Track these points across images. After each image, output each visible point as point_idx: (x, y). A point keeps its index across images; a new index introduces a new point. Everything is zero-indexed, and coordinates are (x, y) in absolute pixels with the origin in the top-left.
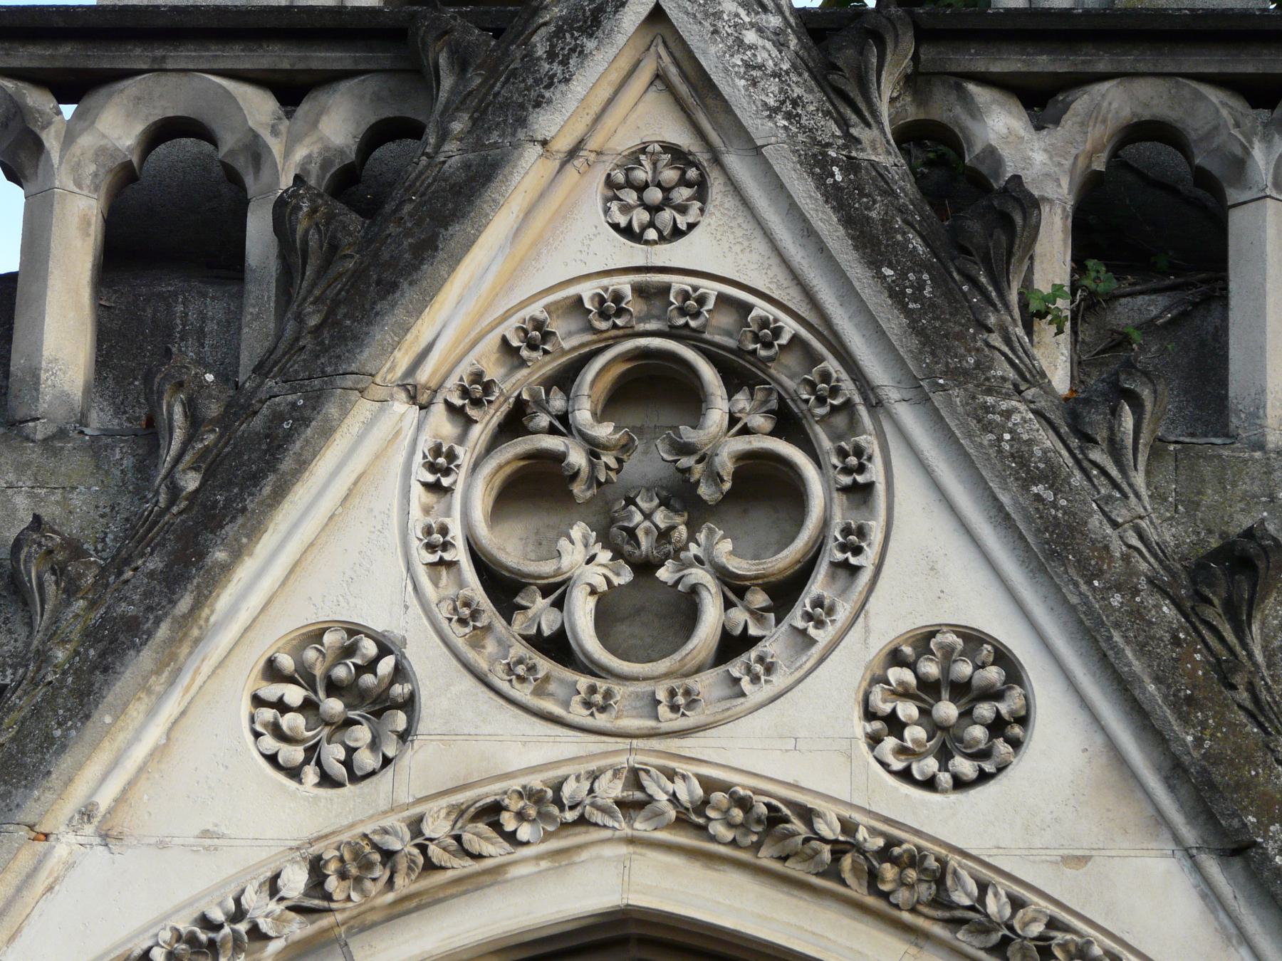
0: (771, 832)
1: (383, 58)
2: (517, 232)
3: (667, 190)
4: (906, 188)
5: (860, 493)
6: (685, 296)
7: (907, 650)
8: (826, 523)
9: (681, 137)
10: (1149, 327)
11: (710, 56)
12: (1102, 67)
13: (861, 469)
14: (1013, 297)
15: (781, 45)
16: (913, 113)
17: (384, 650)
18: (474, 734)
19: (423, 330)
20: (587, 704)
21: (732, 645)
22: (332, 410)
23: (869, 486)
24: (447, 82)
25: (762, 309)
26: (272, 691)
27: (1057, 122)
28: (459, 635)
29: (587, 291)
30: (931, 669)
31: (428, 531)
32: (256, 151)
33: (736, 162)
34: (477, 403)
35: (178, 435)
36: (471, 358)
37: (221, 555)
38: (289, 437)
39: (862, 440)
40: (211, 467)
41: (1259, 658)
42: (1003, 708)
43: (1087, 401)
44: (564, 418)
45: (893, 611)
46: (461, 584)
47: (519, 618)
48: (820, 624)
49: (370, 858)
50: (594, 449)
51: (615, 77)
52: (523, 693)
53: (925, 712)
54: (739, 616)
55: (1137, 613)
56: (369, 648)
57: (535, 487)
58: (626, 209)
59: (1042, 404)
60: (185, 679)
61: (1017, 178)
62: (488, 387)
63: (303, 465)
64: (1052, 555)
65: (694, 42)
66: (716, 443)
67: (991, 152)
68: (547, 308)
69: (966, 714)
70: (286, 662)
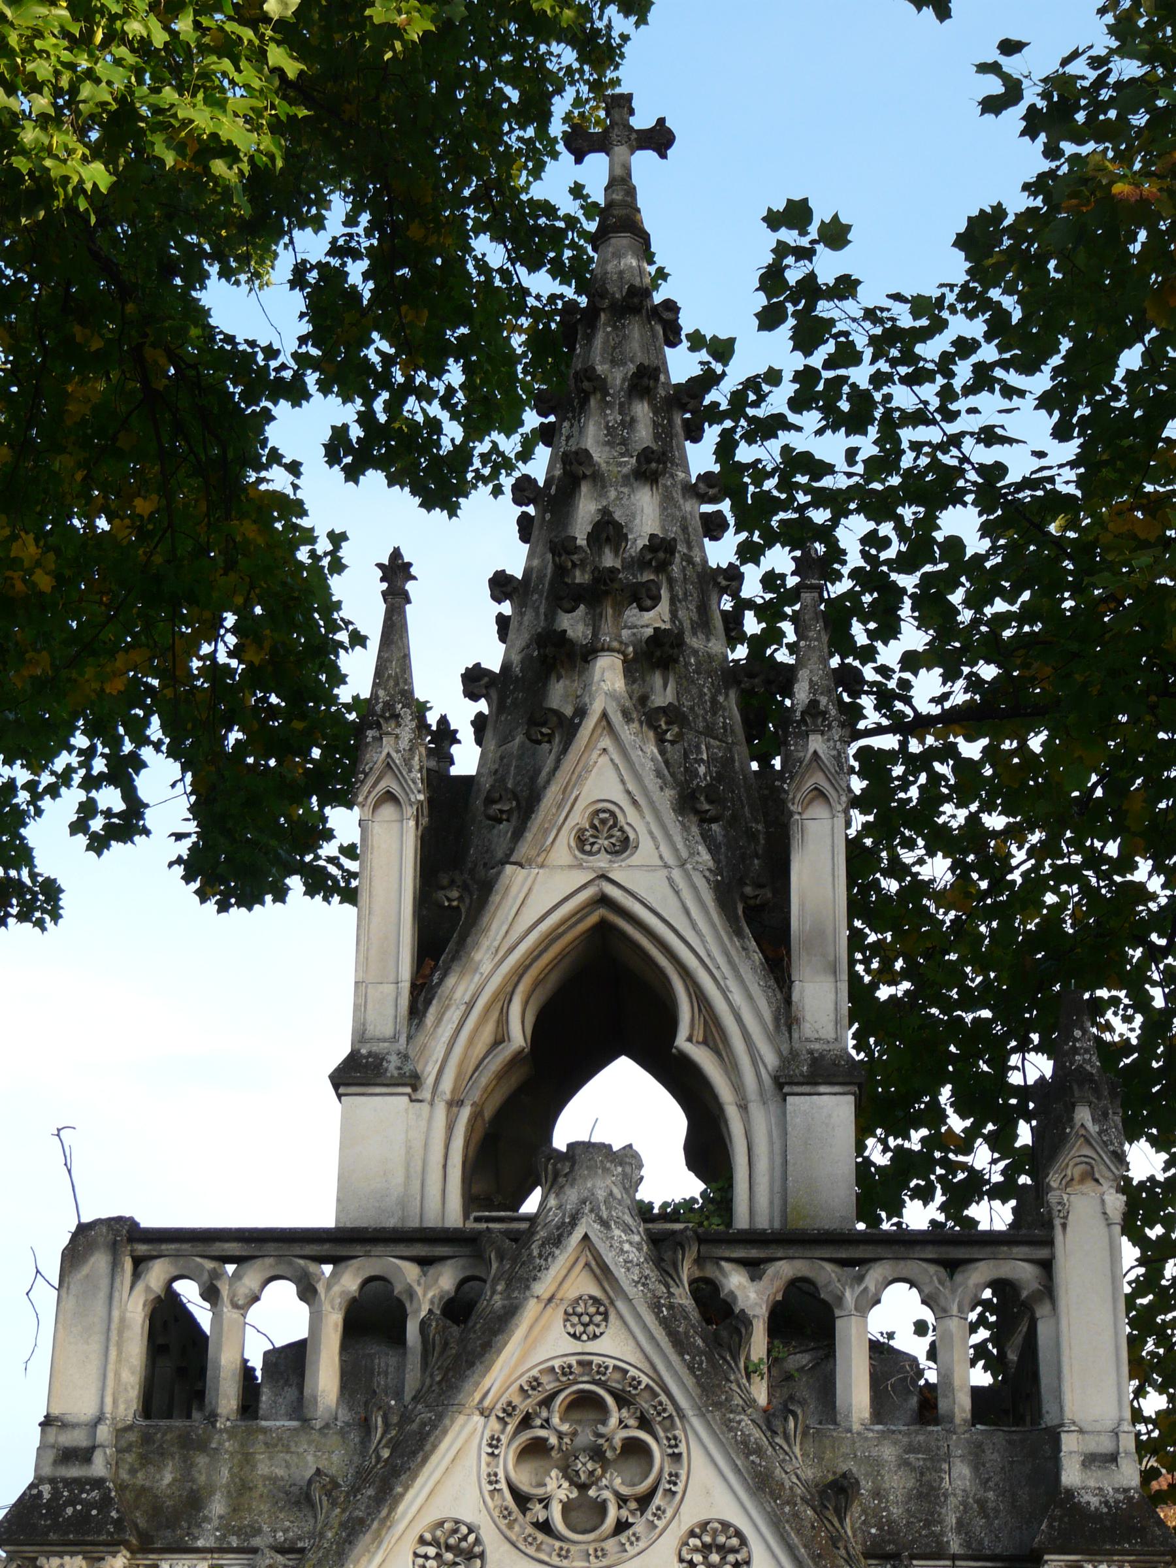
1: (466, 1250)
2: (526, 1337)
3: (591, 1317)
4: (695, 1315)
5: (676, 1457)
6: (599, 1366)
7: (697, 1530)
8: (661, 1470)
9: (597, 1292)
10: (801, 1369)
11: (609, 1258)
12: (779, 1255)
13: (676, 1446)
14: (742, 1365)
15: (639, 1250)
16: (697, 1274)
17: (471, 1531)
19: (487, 1382)
20: (559, 1555)
21: (622, 1526)
22: (447, 1421)
23: (680, 1454)
24: (495, 1265)
25: (633, 1372)
26: (422, 1550)
27: (760, 1279)
28: (503, 1523)
29: (557, 1363)
30: (707, 1539)
31: (489, 1475)
32: (411, 1294)
33: (620, 1304)
34: (509, 1415)
35: (380, 1431)
36: (507, 1395)
37: (399, 1490)
38: (429, 1434)
39: (677, 1432)
40: (395, 1446)
41: (850, 1533)
42: (739, 1557)
43: (774, 1415)
44: (547, 1421)
45: (691, 1513)
46: (504, 1499)
47: (528, 1514)
48: (659, 1518)
50: (561, 1436)
51: (568, 1264)
52: (531, 1551)
53: (705, 1558)
54: (624, 1513)
55: (796, 1515)
56: (464, 1530)
57: (535, 1450)
58: (573, 1325)
59: (754, 1416)
60: (384, 1546)
61: (743, 1311)
62: (514, 1408)
63: (435, 1447)
64: (759, 1488)
65: (602, 1251)
66: (614, 1432)
67: (732, 1293)
68: (541, 1372)
69: (723, 1558)
70: (428, 1536)
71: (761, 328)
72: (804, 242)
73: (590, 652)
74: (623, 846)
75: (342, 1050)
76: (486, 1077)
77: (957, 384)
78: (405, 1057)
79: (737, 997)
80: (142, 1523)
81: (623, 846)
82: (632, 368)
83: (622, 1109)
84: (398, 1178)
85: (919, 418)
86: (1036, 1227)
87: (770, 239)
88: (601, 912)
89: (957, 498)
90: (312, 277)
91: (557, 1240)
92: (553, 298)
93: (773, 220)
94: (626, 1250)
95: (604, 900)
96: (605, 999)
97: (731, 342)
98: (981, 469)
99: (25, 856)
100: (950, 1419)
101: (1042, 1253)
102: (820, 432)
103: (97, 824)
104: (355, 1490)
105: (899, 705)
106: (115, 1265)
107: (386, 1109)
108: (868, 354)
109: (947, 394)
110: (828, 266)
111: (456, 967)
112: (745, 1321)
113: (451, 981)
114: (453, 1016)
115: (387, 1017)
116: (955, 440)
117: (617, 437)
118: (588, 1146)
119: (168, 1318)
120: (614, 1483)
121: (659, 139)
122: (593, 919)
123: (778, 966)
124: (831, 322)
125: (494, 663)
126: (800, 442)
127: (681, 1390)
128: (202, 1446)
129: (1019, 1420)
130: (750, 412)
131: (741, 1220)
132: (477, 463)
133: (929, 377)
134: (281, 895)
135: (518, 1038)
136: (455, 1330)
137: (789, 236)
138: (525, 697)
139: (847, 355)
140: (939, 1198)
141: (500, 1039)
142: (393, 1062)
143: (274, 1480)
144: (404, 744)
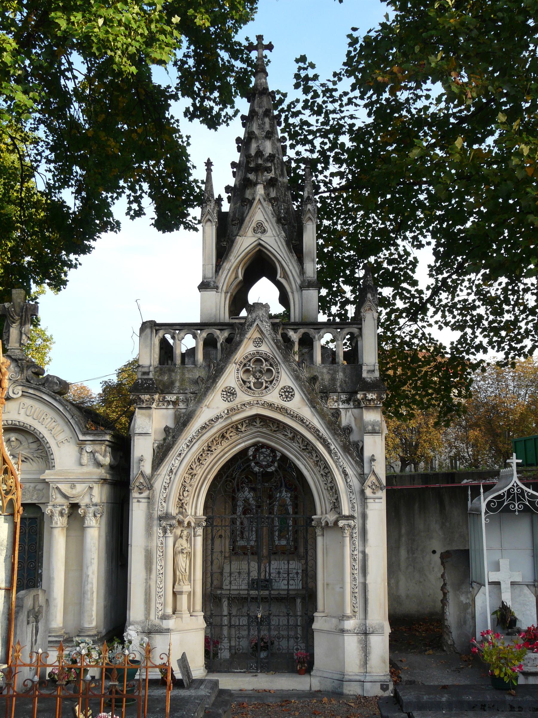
0: (270, 406)
4: (282, 341)
11: (263, 329)
18: (242, 397)
21: (266, 387)
32: (218, 337)
40: (216, 371)
45: (281, 385)
49: (233, 409)
71: (295, 88)
72: (305, 66)
73: (256, 184)
74: (264, 231)
75: (200, 281)
76: (233, 287)
77: (344, 103)
78: (215, 282)
79: (291, 267)
80: (161, 388)
81: (264, 231)
82: (264, 109)
83: (264, 292)
84: (214, 310)
85: (334, 112)
86: (358, 320)
87: (297, 66)
88: (259, 247)
89: (344, 133)
90: (179, 63)
91: (251, 325)
92: (241, 68)
93: (297, 61)
94: (266, 327)
95: (260, 244)
96: (260, 265)
97: (286, 93)
98: (349, 125)
99: (110, 214)
100: (338, 363)
101: (360, 326)
102: (310, 116)
103: (132, 213)
104: (208, 380)
105: (329, 185)
106: (152, 332)
107: (211, 294)
108: (321, 95)
109: (341, 106)
110: (311, 73)
111: (226, 261)
112: (293, 343)
113: (225, 264)
114: (225, 272)
115: (210, 273)
116: (343, 118)
117: (261, 127)
118: (258, 303)
119: (164, 342)
120: (264, 378)
121: (270, 47)
122: (257, 249)
123: (300, 260)
124: (312, 87)
125: (232, 185)
126: (305, 118)
127: (279, 358)
128: (173, 371)
129: (354, 363)
130: (292, 110)
131: (292, 320)
132: (223, 118)
133: (337, 101)
134: (178, 229)
135: (240, 277)
136: (229, 345)
137: (301, 65)
138: (239, 193)
139: (316, 95)
140: (339, 305)
141: (236, 277)
142: (212, 283)
143: (189, 378)
144: (212, 207)
